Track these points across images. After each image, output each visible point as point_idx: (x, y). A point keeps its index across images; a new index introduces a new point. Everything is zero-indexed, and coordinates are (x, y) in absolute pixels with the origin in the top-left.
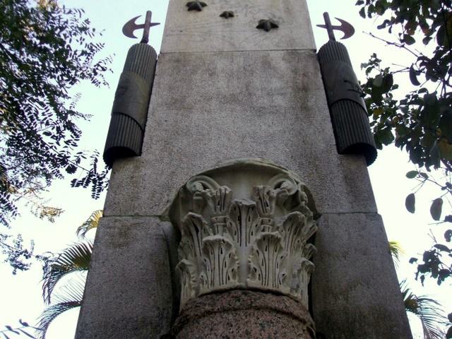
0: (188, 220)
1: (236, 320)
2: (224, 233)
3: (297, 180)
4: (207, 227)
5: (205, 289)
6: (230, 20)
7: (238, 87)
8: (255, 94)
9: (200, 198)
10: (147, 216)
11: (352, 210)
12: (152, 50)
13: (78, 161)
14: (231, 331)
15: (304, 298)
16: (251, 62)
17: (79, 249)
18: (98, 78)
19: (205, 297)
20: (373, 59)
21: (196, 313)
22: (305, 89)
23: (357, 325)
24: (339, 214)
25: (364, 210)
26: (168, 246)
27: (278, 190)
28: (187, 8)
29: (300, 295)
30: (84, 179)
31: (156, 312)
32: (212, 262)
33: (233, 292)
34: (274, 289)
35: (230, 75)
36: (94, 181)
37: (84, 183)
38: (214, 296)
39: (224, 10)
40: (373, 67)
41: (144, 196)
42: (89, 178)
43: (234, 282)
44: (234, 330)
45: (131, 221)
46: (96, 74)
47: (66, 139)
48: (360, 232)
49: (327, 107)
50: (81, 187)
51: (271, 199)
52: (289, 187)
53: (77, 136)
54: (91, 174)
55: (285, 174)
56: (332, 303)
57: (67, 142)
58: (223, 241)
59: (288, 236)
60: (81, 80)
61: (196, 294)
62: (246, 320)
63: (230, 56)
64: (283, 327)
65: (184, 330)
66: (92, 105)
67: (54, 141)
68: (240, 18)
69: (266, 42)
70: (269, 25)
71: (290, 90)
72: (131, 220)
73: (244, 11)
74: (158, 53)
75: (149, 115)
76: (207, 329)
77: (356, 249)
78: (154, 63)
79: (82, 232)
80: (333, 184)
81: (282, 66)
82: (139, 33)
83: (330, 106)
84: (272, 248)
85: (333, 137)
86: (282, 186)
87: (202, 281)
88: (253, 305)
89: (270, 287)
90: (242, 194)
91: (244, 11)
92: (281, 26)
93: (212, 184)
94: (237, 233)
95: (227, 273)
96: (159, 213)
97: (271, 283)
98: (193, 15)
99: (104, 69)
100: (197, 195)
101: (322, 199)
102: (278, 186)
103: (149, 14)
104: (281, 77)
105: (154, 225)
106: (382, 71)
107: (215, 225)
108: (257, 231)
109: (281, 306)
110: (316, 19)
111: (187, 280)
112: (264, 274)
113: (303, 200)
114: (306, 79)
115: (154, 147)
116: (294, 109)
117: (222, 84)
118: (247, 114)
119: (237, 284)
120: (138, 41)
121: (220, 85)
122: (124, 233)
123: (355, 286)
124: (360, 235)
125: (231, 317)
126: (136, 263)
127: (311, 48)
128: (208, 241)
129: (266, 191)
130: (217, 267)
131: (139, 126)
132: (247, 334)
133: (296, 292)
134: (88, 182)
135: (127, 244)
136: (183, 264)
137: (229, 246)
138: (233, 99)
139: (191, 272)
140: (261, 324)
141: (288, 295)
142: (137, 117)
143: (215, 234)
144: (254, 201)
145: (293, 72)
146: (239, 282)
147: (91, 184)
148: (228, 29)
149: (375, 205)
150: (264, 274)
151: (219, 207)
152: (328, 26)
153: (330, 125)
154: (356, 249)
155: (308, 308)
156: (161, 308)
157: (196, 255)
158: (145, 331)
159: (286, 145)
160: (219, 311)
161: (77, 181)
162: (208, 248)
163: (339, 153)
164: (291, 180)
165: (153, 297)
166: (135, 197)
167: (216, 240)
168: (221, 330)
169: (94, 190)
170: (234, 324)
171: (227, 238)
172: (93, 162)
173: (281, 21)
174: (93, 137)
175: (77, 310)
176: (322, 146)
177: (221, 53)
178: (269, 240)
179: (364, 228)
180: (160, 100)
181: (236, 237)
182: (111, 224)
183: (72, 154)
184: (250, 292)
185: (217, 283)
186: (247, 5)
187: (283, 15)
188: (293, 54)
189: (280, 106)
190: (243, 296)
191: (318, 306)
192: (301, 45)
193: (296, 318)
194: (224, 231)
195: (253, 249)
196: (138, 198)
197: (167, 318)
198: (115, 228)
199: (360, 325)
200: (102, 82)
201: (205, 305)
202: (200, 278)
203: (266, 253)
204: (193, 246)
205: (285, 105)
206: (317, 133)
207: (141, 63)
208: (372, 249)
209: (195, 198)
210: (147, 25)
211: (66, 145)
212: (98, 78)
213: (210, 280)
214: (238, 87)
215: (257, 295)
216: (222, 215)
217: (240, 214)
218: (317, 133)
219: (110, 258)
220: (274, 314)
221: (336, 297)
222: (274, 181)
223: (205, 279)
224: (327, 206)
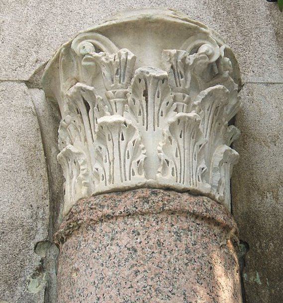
0: (75, 93)
3: (220, 41)
5: (100, 186)
14: (139, 241)
19: (102, 196)
21: (91, 217)
24: (267, 84)
31: (28, 212)
32: (111, 151)
33: (140, 190)
38: (114, 195)
43: (139, 179)
44: (143, 240)
55: (205, 33)
56: (258, 202)
58: (125, 124)
61: (88, 192)
62: (157, 227)
65: (74, 238)
76: (106, 238)
87: (97, 175)
88: (167, 208)
100: (87, 60)
111: (75, 173)
125: (137, 223)
128: (105, 123)
132: (159, 245)
136: (69, 151)
139: (80, 162)
141: (208, 195)
143: (112, 114)
144: (164, 70)
156: (35, 206)
157: (86, 140)
158: (15, 236)
164: (211, 42)
167: (115, 122)
168: (124, 239)
170: (141, 232)
171: (130, 119)
181: (140, 118)
190: (153, 197)
197: (43, 219)
201: (102, 207)
213: (107, 174)
216: (122, 88)
217: (146, 87)
220: (192, 219)
221: (263, 195)
223: (101, 173)
224: (252, 73)
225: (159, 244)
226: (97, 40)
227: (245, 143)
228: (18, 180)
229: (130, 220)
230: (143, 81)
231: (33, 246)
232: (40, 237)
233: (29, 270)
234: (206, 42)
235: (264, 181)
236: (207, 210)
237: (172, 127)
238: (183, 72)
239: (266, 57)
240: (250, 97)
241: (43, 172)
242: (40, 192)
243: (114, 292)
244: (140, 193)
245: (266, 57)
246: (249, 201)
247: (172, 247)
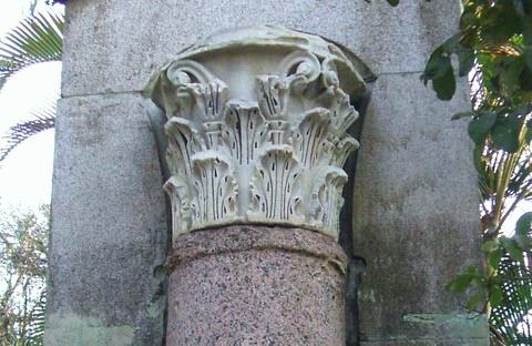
1: (234, 264)
2: (220, 147)
4: (197, 137)
5: (198, 223)
9: (186, 94)
10: (123, 92)
15: (331, 226)
17: (34, 26)
23: (411, 244)
24: (404, 74)
27: (293, 77)
29: (320, 222)
31: (147, 236)
34: (283, 221)
38: (208, 232)
41: (117, 58)
43: (231, 216)
45: (102, 102)
48: (431, 103)
51: (281, 93)
52: (308, 72)
55: (304, 50)
56: (380, 214)
59: (306, 142)
61: (189, 227)
72: (102, 101)
77: (422, 133)
80: (401, 22)
84: (281, 166)
86: (298, 72)
88: (255, 245)
89: (278, 220)
90: (241, 89)
94: (235, 146)
95: (219, 183)
96: (141, 87)
97: (278, 214)
100: (182, 91)
101: (381, 49)
102: (293, 70)
107: (208, 134)
108: (262, 142)
109: (291, 244)
112: (269, 202)
113: (330, 84)
119: (236, 218)
122: (94, 122)
123: (414, 189)
124: (432, 110)
125: (228, 260)
129: (273, 83)
130: (210, 195)
133: (316, 218)
135: (100, 138)
137: (224, 166)
139: (181, 196)
141: (302, 227)
146: (239, 214)
150: (269, 202)
151: (210, 109)
154: (422, 133)
156: (153, 229)
160: (213, 253)
162: (199, 168)
165: (141, 216)
166: (103, 63)
168: (216, 276)
171: (224, 154)
175: (49, 134)
178: (276, 156)
181: (234, 151)
182: (74, 110)
184: (251, 228)
185: (211, 217)
191: (360, 220)
193: (312, 254)
194: (220, 143)
195: (255, 168)
196: (107, 64)
197: (161, 243)
198: (79, 114)
199: (415, 244)
201: (197, 244)
202: (198, 206)
203: (273, 173)
204: (182, 159)
209: (179, 94)
215: (260, 231)
219: (79, 162)
221: (386, 206)
222: (289, 62)
223: (197, 210)
224: (387, 62)
225: (247, 280)
226: (192, 67)
227: (372, 149)
229: (221, 258)
230: (234, 113)
231: (152, 270)
232: (158, 262)
233: (149, 295)
234: (306, 59)
235: (390, 191)
236: (298, 243)
237: (310, 118)
238: (277, 99)
239: (406, 40)
240: (382, 92)
243: (205, 326)
244: (230, 231)
245: (406, 40)
246: (370, 214)
247: (259, 282)
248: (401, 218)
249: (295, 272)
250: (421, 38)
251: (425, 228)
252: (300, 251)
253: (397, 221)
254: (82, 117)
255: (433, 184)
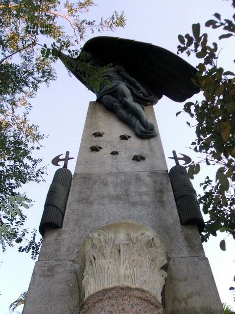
1: (116, 303)
6: (116, 156)
7: (121, 191)
8: (131, 195)
11: (189, 255)
12: (70, 172)
13: (24, 235)
16: (129, 178)
18: (39, 178)
20: (207, 180)
22: (161, 191)
24: (182, 257)
25: (196, 255)
26: (77, 276)
28: (90, 150)
30: (27, 247)
35: (116, 185)
36: (33, 248)
37: (27, 249)
39: (113, 151)
40: (208, 185)
41: (64, 250)
42: (30, 246)
46: (37, 175)
47: (17, 220)
49: (174, 200)
50: (24, 252)
53: (24, 219)
54: (31, 243)
56: (177, 305)
57: (17, 223)
60: (28, 181)
63: (117, 175)
64: (144, 308)
66: (35, 194)
67: (9, 222)
68: (122, 155)
69: (138, 167)
70: (127, 137)
71: (152, 192)
73: (125, 151)
74: (73, 174)
75: (67, 207)
78: (70, 179)
79: (13, 307)
81: (148, 180)
82: (62, 164)
83: (176, 200)
85: (178, 217)
91: (125, 151)
92: (147, 159)
93: (103, 234)
95: (112, 279)
96: (72, 259)
98: (94, 154)
99: (42, 173)
100: (96, 240)
102: (142, 234)
103: (68, 153)
104: (147, 186)
105: (69, 265)
106: (213, 187)
110: (168, 154)
114: (162, 186)
115: (70, 223)
116: (154, 202)
117: (111, 190)
118: (127, 205)
120: (62, 167)
121: (110, 191)
122: (51, 269)
126: (57, 286)
127: (165, 169)
131: (61, 212)
134: (29, 249)
135: (52, 275)
138: (118, 198)
140: (131, 305)
142: (60, 207)
145: (154, 182)
147: (31, 250)
148: (115, 161)
149: (204, 252)
152: (175, 158)
153: (176, 210)
155: (161, 302)
156: (72, 310)
159: (150, 221)
161: (22, 248)
163: (182, 225)
166: (58, 250)
169: (33, 254)
172: (33, 236)
173: (147, 155)
174: (34, 216)
176: (172, 221)
177: (110, 174)
179: (197, 265)
180: (74, 199)
182: (43, 265)
183: (20, 229)
186: (126, 148)
187: (148, 153)
188: (154, 173)
189: (146, 201)
191: (169, 307)
192: (159, 168)
196: (60, 251)
200: (41, 180)
205: (149, 200)
206: (168, 215)
207: (62, 179)
208: (202, 276)
210: (67, 159)
211: (16, 224)
212: (39, 178)
214: (121, 191)
218: (168, 215)
221: (180, 302)
225: (123, 309)
228: (66, 300)
236: (147, 297)
241: (77, 296)
242: (75, 304)
245: (181, 247)
248: (187, 307)
249: (146, 309)
250: (187, 247)
251: (199, 310)
252: (147, 301)
253: (185, 308)
254: (46, 268)
255: (199, 294)
